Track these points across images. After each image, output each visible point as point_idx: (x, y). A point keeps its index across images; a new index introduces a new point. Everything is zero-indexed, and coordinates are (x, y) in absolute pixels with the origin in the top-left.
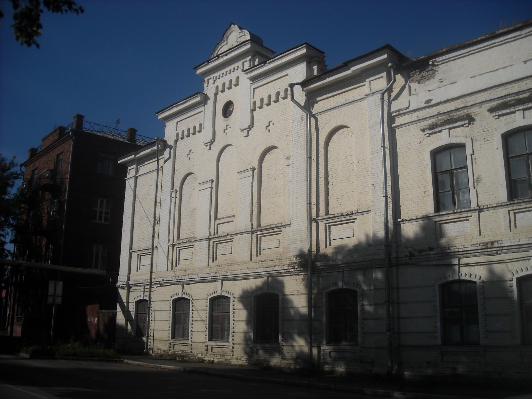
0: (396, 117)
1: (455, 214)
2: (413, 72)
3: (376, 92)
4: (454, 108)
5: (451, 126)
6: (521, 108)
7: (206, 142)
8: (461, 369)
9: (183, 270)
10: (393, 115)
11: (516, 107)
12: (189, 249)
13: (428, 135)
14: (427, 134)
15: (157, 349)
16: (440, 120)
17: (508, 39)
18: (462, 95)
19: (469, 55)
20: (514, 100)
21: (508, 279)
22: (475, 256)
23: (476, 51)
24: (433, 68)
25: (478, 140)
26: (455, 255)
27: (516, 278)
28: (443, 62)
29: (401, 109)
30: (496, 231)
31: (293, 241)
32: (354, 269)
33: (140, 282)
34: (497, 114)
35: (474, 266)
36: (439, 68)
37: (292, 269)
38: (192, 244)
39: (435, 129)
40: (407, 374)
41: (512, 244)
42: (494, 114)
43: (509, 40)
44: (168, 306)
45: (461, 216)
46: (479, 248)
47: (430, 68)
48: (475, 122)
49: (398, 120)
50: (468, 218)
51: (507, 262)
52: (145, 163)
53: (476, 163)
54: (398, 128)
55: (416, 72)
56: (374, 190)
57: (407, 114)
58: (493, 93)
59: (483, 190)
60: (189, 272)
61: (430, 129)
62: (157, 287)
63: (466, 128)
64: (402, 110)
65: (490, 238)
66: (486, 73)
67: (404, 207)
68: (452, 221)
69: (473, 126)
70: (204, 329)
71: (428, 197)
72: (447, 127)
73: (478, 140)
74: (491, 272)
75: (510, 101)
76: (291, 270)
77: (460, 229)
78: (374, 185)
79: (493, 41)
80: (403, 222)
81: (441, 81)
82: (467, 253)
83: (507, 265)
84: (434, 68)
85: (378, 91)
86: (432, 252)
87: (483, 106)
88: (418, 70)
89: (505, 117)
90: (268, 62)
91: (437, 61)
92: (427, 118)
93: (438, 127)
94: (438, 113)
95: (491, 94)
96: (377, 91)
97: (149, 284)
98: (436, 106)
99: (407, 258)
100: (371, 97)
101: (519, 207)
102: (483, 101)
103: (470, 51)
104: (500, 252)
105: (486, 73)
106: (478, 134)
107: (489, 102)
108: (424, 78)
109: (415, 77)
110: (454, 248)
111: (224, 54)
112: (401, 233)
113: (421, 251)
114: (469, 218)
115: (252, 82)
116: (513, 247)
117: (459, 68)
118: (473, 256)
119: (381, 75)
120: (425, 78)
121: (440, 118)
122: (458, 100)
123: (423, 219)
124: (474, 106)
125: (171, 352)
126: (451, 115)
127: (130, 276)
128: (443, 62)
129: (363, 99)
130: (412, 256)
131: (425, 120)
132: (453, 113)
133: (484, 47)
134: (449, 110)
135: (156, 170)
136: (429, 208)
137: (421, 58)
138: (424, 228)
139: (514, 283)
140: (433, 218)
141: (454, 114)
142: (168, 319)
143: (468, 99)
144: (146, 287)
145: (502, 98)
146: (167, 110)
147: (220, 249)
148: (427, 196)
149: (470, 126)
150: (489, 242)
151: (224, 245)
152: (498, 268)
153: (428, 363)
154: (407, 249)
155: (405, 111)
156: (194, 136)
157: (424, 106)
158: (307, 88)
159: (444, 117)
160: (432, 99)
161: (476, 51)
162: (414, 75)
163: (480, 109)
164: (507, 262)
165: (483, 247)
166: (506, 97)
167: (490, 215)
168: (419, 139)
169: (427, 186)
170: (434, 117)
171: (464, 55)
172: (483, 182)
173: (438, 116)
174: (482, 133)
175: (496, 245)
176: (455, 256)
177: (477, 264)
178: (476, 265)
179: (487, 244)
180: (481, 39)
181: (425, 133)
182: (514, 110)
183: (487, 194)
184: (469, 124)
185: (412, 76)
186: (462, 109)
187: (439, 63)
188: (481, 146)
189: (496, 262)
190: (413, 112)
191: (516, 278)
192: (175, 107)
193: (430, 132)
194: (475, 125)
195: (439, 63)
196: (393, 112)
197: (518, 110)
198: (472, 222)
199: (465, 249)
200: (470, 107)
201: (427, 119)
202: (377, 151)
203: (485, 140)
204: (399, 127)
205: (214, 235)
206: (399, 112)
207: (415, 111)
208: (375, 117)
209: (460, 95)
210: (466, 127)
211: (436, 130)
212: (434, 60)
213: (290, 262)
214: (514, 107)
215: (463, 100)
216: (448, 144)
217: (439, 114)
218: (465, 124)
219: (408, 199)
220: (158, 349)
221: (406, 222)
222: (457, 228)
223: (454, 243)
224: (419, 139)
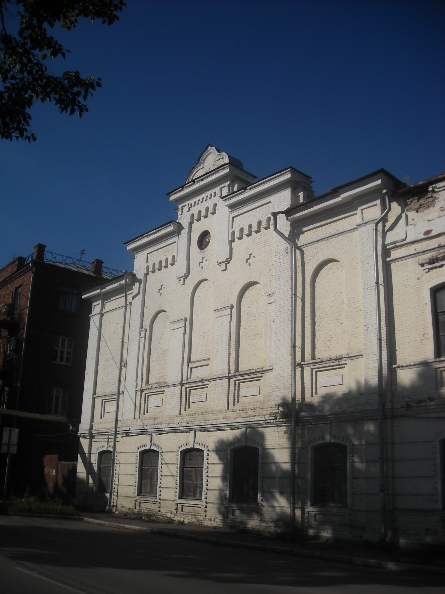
2: (411, 199)
3: (369, 222)
7: (179, 277)
9: (152, 418)
10: (388, 247)
12: (159, 395)
14: (426, 269)
15: (121, 506)
16: (441, 253)
31: (275, 388)
33: (104, 431)
37: (273, 419)
38: (162, 390)
44: (134, 459)
47: (429, 195)
52: (112, 299)
54: (393, 262)
55: (414, 199)
56: (367, 332)
57: (404, 246)
60: (158, 421)
61: (429, 263)
62: (122, 437)
67: (400, 351)
70: (174, 486)
76: (272, 421)
80: (398, 369)
81: (442, 209)
84: (434, 195)
85: (371, 221)
86: (432, 403)
88: (416, 198)
90: (248, 188)
91: (437, 187)
92: (427, 251)
93: (439, 261)
97: (113, 433)
99: (404, 409)
109: (413, 204)
111: (200, 179)
113: (420, 402)
119: (375, 203)
123: (416, 366)
125: (136, 510)
127: (93, 424)
129: (354, 230)
130: (409, 406)
135: (124, 306)
137: (419, 183)
138: (421, 376)
144: (110, 437)
146: (137, 241)
147: (194, 395)
148: (426, 339)
151: (198, 391)
155: (401, 243)
156: (46, 246)
158: (292, 217)
160: (432, 230)
162: (411, 202)
169: (426, 328)
173: (439, 249)
185: (409, 204)
187: (440, 190)
190: (411, 244)
192: (146, 237)
193: (430, 266)
195: (440, 190)
196: (388, 245)
201: (426, 252)
202: (370, 288)
204: (395, 261)
205: (187, 380)
206: (395, 244)
207: (413, 243)
211: (437, 264)
212: (434, 185)
213: (272, 411)
220: (123, 507)
221: (402, 368)
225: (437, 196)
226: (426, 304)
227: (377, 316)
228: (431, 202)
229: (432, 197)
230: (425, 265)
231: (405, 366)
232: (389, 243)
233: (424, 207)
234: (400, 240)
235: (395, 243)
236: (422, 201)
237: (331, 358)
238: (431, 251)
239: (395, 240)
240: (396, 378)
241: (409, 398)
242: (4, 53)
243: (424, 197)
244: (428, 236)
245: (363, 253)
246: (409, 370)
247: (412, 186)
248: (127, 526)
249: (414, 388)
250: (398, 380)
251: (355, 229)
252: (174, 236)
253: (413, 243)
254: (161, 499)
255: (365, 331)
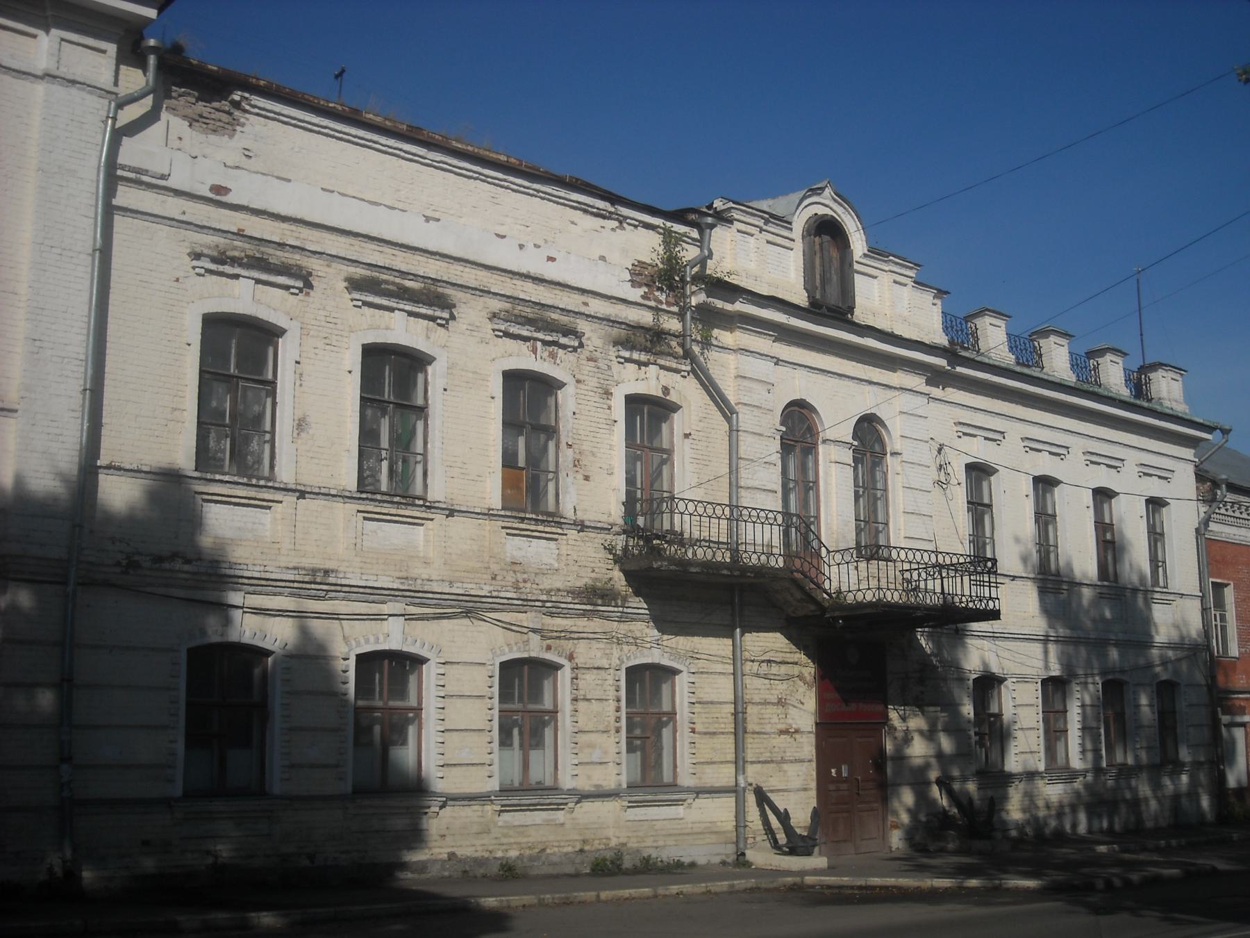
0: (122, 181)
1: (248, 488)
2: (183, 90)
3: (84, 84)
4: (276, 239)
5: (264, 277)
6: (408, 308)
8: (224, 850)
10: (119, 172)
11: (401, 301)
13: (202, 271)
14: (202, 268)
16: (235, 248)
17: (400, 150)
18: (299, 217)
19: (319, 133)
20: (393, 283)
21: (338, 654)
22: (280, 594)
23: (337, 134)
24: (232, 111)
25: (313, 336)
26: (238, 583)
27: (357, 656)
28: (263, 113)
29: (147, 171)
30: (326, 548)
32: (720, 625)
34: (363, 298)
35: (275, 616)
36: (247, 119)
39: (226, 267)
40: (87, 875)
41: (363, 584)
42: (356, 295)
43: (402, 154)
44: (485, 682)
45: (260, 496)
46: (298, 578)
47: (225, 105)
48: (312, 293)
49: (125, 192)
50: (270, 504)
51: (344, 619)
53: (301, 385)
54: (122, 213)
55: (189, 94)
56: (36, 356)
57: (155, 190)
58: (357, 248)
59: (309, 451)
61: (214, 260)
63: (291, 296)
64: (149, 174)
65: (315, 561)
66: (354, 197)
67: (111, 431)
68: (233, 500)
69: (307, 298)
71: (180, 424)
72: (256, 274)
73: (313, 336)
74: (304, 633)
75: (387, 282)
77: (245, 523)
78: (37, 343)
79: (375, 137)
80: (105, 471)
81: (247, 153)
82: (265, 584)
83: (341, 624)
84: (237, 113)
85: (89, 86)
86: (186, 567)
87: (334, 265)
88: (196, 94)
89: (372, 309)
91: (252, 103)
92: (210, 228)
93: (236, 265)
94: (239, 230)
95: (352, 248)
96: (88, 82)
98: (230, 210)
99: (118, 570)
100: (60, 88)
101: (378, 510)
102: (340, 255)
103: (325, 127)
104: (333, 594)
105: (354, 197)
106: (314, 322)
107: (349, 263)
108: (204, 120)
109: (182, 103)
110: (242, 567)
112: (96, 499)
113: (159, 559)
114: (275, 504)
115: (866, 252)
116: (361, 590)
117: (293, 149)
118: (275, 594)
119: (103, 45)
120: (208, 121)
121: (236, 243)
122: (283, 222)
123: (149, 476)
124: (317, 256)
126: (262, 249)
128: (263, 113)
129: (24, 76)
130: (132, 565)
131: (199, 230)
132: (268, 247)
133: (355, 137)
134: (265, 237)
136: (182, 454)
137: (210, 67)
138: (154, 497)
139: (352, 663)
140: (194, 481)
141: (270, 251)
142: (486, 691)
143: (306, 232)
145: (374, 269)
148: (178, 422)
149: (301, 296)
150: (319, 570)
152: (317, 626)
153: (146, 843)
154: (113, 543)
155: (154, 181)
157: (204, 194)
159: (247, 246)
161: (337, 134)
162: (180, 96)
163: (327, 269)
164: (344, 619)
165: (307, 579)
166: (383, 270)
167: (926, 580)
168: (175, 269)
170: (225, 235)
171: (310, 126)
172: (311, 432)
173: (235, 237)
174: (323, 323)
175: (332, 580)
176: (235, 586)
177: (281, 613)
178: (279, 616)
179: (314, 571)
180: (335, 107)
181: (195, 263)
182: (395, 305)
183: (316, 461)
184: (301, 290)
185: (174, 98)
186: (291, 250)
187: (252, 110)
188: (317, 351)
189: (320, 615)
190: (172, 194)
191: (357, 656)
193: (213, 267)
194: (310, 299)
195: (252, 110)
196: (123, 168)
197: (399, 310)
198: (278, 516)
199: (268, 576)
200: (309, 254)
201: (206, 231)
202: (59, 251)
203: (327, 341)
204: (128, 214)
206: (138, 176)
207: (178, 193)
208: (64, 149)
209: (294, 216)
210: (292, 294)
211: (227, 269)
212: (247, 95)
214: (397, 300)
215: (293, 228)
216: (250, 316)
217: (240, 234)
218: (293, 287)
219: (126, 413)
221: (115, 472)
222: (240, 521)
223: (236, 554)
224: (175, 269)
225: (242, 120)
226: (189, 345)
227: (96, 207)
228: (225, 123)
229: (230, 113)
230: (202, 258)
231: (126, 470)
232: (126, 166)
233: (207, 124)
234: (155, 173)
235: (141, 171)
236: (201, 107)
237: (243, 231)
238: (216, 233)
239: (144, 167)
240: (97, 492)
241: (128, 544)
242: (565, 352)
243: (210, 102)
244: (218, 198)
245: (50, 152)
246: (129, 480)
247: (195, 62)
248: (1200, 861)
249: (130, 520)
250: (100, 495)
251: (30, 77)
252: (98, 175)
253: (178, 193)
254: (696, 730)
255: (33, 353)
